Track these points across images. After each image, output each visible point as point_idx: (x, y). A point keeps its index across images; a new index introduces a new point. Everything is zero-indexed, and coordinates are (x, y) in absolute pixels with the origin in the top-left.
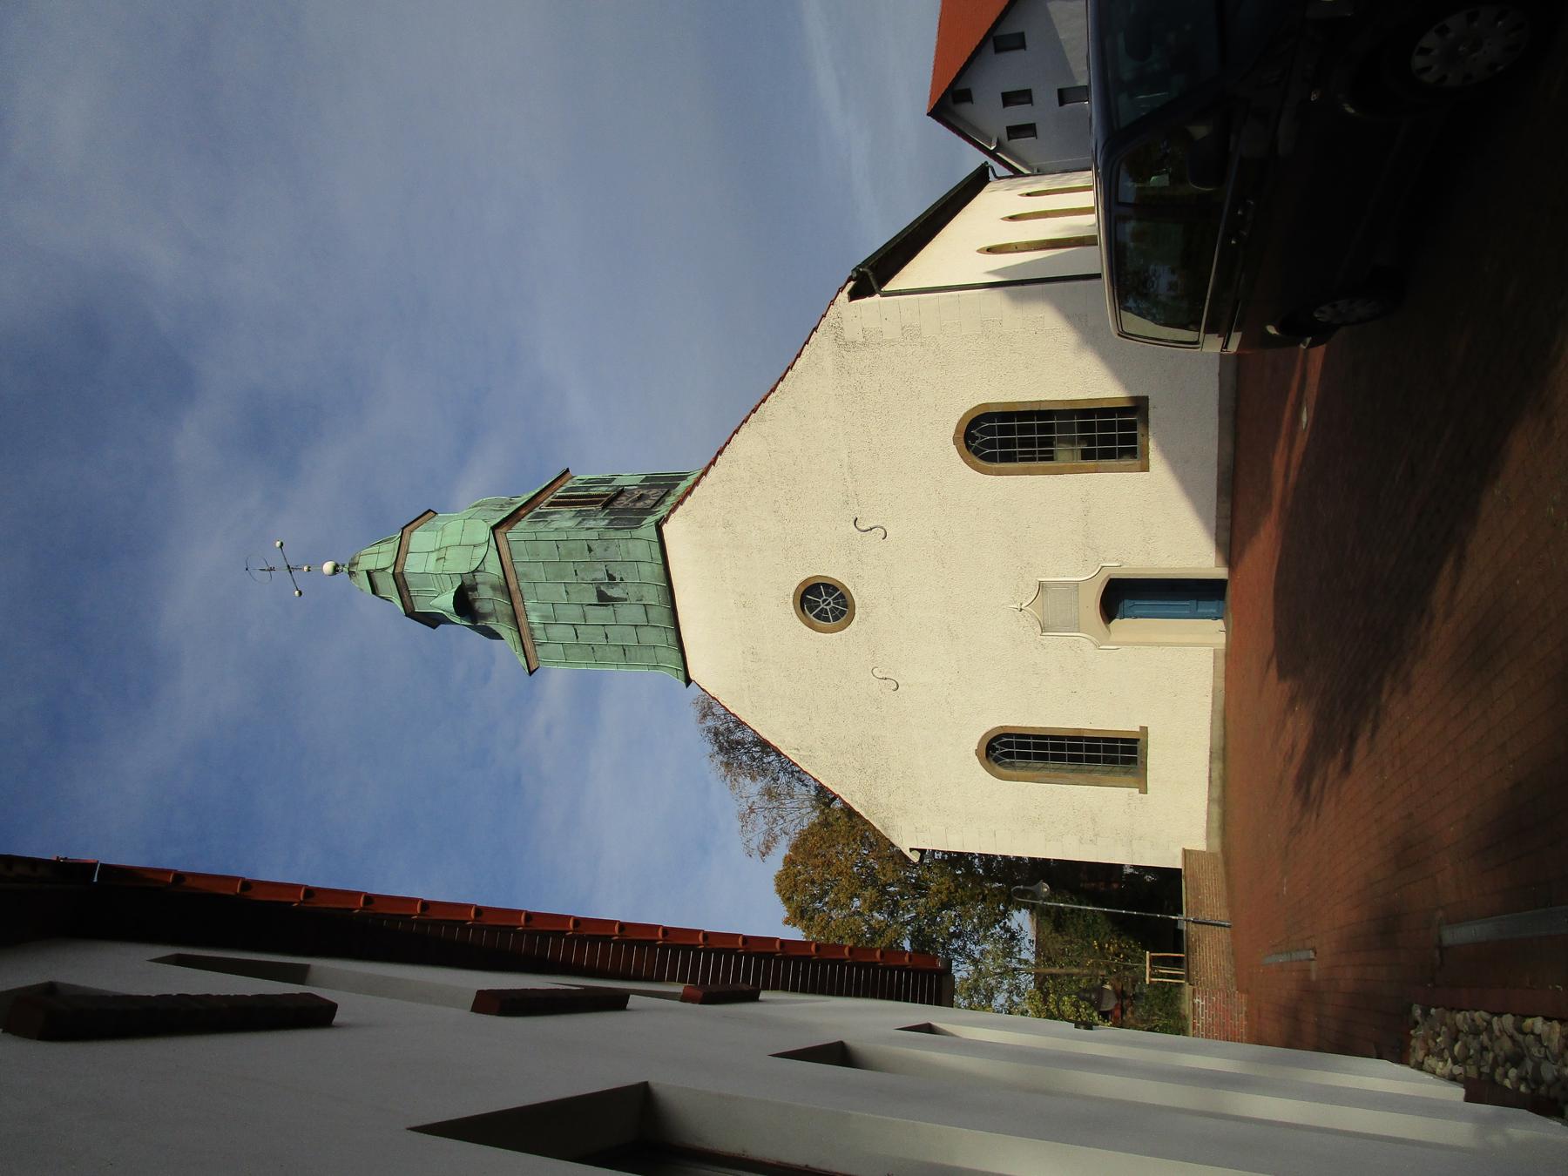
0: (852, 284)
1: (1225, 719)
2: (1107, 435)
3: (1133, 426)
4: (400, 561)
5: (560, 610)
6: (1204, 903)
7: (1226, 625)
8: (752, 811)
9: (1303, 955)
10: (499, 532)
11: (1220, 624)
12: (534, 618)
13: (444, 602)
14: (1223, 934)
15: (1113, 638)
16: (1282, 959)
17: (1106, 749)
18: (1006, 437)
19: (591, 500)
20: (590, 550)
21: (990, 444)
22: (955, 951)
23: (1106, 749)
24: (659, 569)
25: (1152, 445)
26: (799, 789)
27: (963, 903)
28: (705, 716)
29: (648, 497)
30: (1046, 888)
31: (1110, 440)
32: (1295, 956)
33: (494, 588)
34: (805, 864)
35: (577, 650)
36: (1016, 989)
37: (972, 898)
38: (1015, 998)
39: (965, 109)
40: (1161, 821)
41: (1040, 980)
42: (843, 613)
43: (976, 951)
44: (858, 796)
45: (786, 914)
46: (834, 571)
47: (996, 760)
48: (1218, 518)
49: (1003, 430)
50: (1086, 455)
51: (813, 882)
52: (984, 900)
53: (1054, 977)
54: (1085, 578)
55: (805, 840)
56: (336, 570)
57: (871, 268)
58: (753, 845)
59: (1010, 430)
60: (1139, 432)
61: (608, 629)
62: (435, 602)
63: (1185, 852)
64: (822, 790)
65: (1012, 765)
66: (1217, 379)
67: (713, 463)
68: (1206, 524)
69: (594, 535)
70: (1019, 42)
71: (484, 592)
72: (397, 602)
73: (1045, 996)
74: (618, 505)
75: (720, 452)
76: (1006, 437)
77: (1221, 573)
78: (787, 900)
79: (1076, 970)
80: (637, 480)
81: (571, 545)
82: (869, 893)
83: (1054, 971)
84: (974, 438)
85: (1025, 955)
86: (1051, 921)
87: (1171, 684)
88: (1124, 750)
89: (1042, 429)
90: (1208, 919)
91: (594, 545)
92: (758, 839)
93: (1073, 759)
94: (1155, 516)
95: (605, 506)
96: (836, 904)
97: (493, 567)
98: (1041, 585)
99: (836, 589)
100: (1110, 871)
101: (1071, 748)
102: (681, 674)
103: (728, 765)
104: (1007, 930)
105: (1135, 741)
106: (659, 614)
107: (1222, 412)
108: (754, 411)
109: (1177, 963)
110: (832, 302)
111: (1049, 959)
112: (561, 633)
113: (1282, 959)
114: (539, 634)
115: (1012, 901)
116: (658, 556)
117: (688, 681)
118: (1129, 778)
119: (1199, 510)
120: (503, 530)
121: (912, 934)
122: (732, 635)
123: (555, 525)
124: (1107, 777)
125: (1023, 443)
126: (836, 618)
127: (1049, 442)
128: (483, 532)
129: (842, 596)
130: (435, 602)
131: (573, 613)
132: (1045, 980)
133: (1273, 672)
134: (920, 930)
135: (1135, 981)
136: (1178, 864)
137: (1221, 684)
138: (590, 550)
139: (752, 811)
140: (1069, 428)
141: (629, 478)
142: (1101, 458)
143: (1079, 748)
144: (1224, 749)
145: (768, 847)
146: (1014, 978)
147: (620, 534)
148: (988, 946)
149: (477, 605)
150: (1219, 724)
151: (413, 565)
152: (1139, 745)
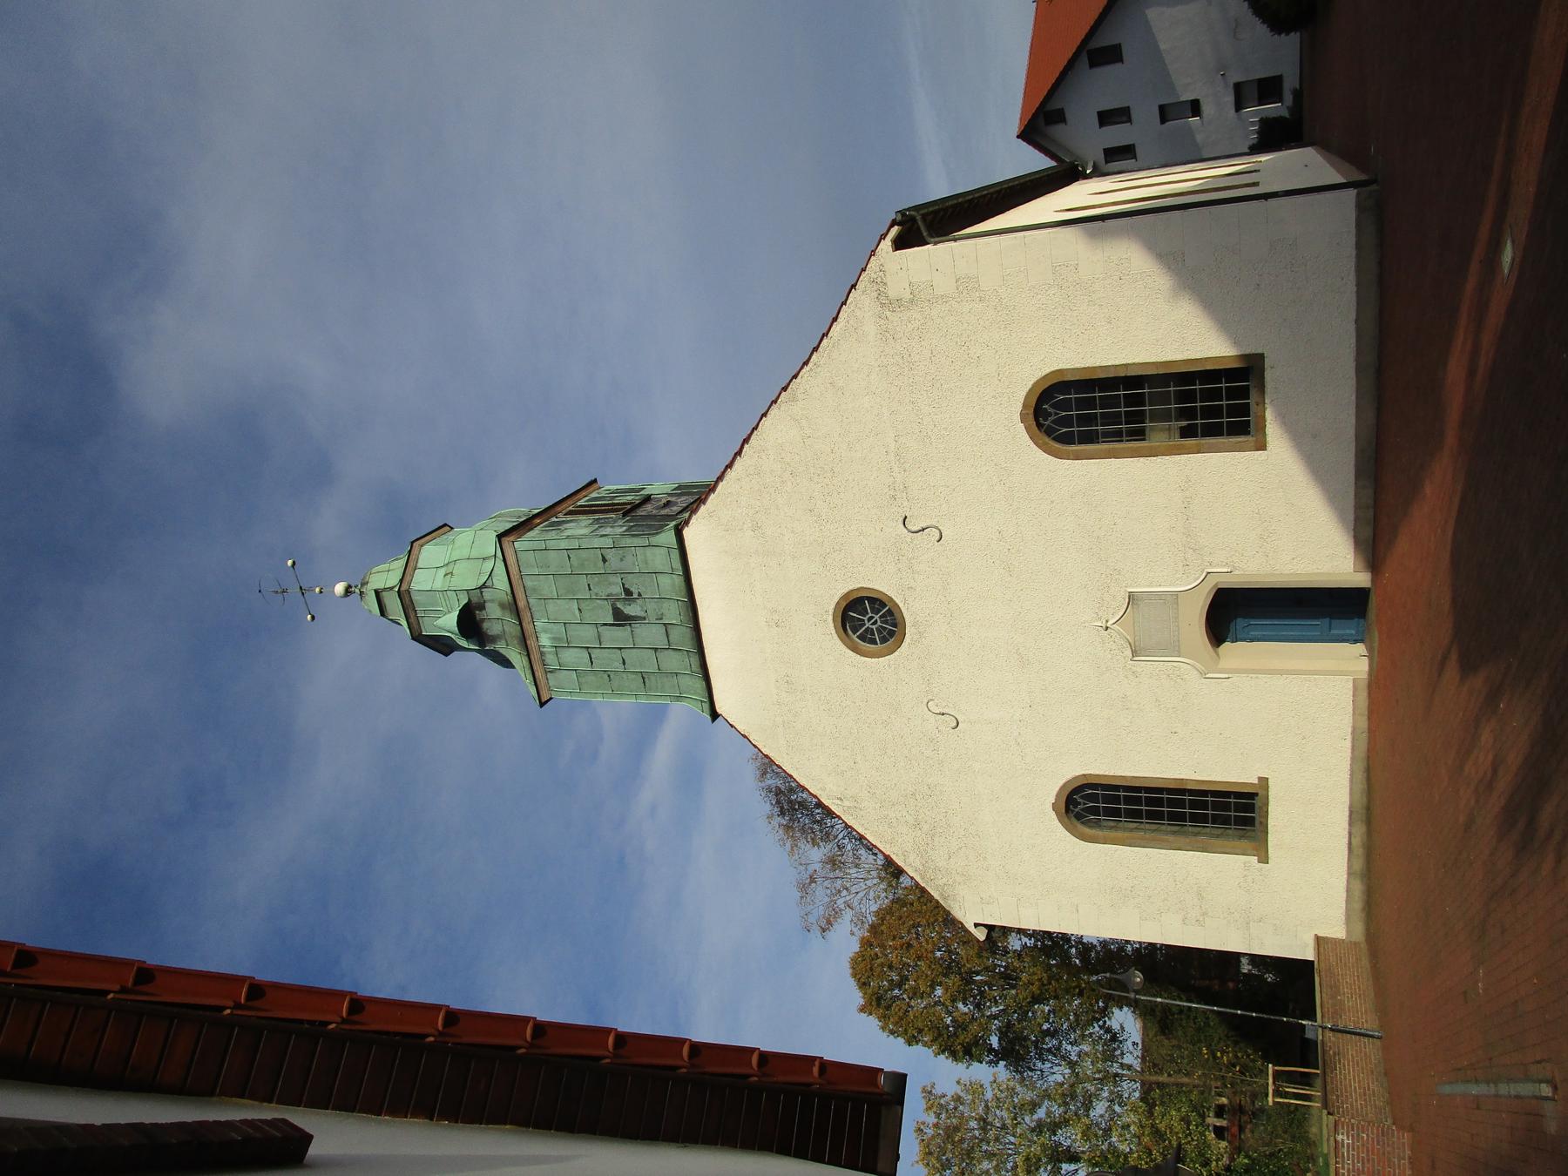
0: (895, 229)
1: (1368, 770)
2: (1209, 405)
3: (1244, 393)
4: (407, 578)
5: (575, 631)
6: (1345, 1004)
7: (1370, 649)
8: (813, 880)
9: (1525, 1089)
11: (1360, 648)
12: (545, 640)
13: (447, 623)
14: (1371, 1049)
15: (1223, 664)
16: (1475, 1090)
17: (1216, 806)
18: (1084, 412)
19: (612, 508)
20: (604, 560)
21: (1066, 421)
22: (1049, 1050)
23: (1216, 806)
24: (679, 581)
25: (1269, 415)
27: (1056, 997)
28: (764, 773)
29: (675, 504)
30: (1138, 978)
32: (1504, 1089)
33: (502, 606)
34: (883, 946)
35: (591, 678)
36: (1116, 1098)
37: (1067, 991)
38: (1117, 1108)
39: (1058, 131)
40: (1290, 898)
41: (1147, 1089)
42: (892, 634)
43: (1073, 1052)
46: (910, 611)
47: (1079, 817)
48: (1357, 507)
49: (1082, 404)
50: (1186, 433)
51: (890, 967)
52: (1081, 994)
53: (1161, 1085)
54: (1189, 583)
55: (883, 919)
56: (348, 591)
57: (924, 217)
58: (812, 919)
59: (1090, 403)
60: (1253, 400)
61: (625, 654)
62: (440, 622)
63: (1318, 939)
64: (889, 861)
65: (1097, 824)
66: (1352, 327)
67: (739, 453)
68: (1342, 518)
69: (608, 542)
70: (1112, 55)
72: (404, 623)
73: (1151, 1107)
74: (641, 512)
75: (746, 441)
76: (1084, 412)
77: (1362, 579)
78: (863, 985)
79: (1186, 1080)
80: (668, 488)
81: (583, 554)
82: (953, 981)
83: (1163, 1078)
84: (1047, 415)
85: (1128, 1059)
86: (1159, 1022)
87: (1298, 722)
88: (1239, 807)
89: (1130, 400)
90: (1351, 1026)
91: (610, 555)
92: (819, 911)
93: (1174, 817)
94: (1275, 508)
95: (624, 515)
96: (915, 993)
97: (501, 582)
100: (1229, 960)
101: (1171, 803)
102: (706, 706)
103: (788, 828)
104: (1108, 1030)
105: (1252, 796)
106: (681, 635)
107: (1359, 369)
108: (785, 389)
109: (1305, 1080)
110: (873, 253)
111: (1155, 1065)
113: (1475, 1090)
114: (551, 659)
115: (1118, 996)
116: (677, 565)
117: (715, 715)
118: (1244, 843)
119: (1332, 498)
120: (512, 538)
121: (999, 1029)
122: (765, 663)
123: (568, 533)
124: (1219, 842)
126: (884, 640)
128: (490, 546)
129: (890, 612)
130: (440, 622)
131: (587, 634)
132: (1150, 1089)
133: (1452, 671)
134: (1009, 1025)
135: (1254, 1096)
137: (1363, 723)
138: (604, 560)
139: (813, 880)
140: (1165, 398)
141: (659, 488)
142: (1204, 435)
143: (1181, 804)
144: (1368, 808)
145: (829, 923)
146: (1115, 1084)
148: (1086, 1048)
149: (485, 625)
150: (1360, 776)
151: (421, 581)
152: (1258, 802)
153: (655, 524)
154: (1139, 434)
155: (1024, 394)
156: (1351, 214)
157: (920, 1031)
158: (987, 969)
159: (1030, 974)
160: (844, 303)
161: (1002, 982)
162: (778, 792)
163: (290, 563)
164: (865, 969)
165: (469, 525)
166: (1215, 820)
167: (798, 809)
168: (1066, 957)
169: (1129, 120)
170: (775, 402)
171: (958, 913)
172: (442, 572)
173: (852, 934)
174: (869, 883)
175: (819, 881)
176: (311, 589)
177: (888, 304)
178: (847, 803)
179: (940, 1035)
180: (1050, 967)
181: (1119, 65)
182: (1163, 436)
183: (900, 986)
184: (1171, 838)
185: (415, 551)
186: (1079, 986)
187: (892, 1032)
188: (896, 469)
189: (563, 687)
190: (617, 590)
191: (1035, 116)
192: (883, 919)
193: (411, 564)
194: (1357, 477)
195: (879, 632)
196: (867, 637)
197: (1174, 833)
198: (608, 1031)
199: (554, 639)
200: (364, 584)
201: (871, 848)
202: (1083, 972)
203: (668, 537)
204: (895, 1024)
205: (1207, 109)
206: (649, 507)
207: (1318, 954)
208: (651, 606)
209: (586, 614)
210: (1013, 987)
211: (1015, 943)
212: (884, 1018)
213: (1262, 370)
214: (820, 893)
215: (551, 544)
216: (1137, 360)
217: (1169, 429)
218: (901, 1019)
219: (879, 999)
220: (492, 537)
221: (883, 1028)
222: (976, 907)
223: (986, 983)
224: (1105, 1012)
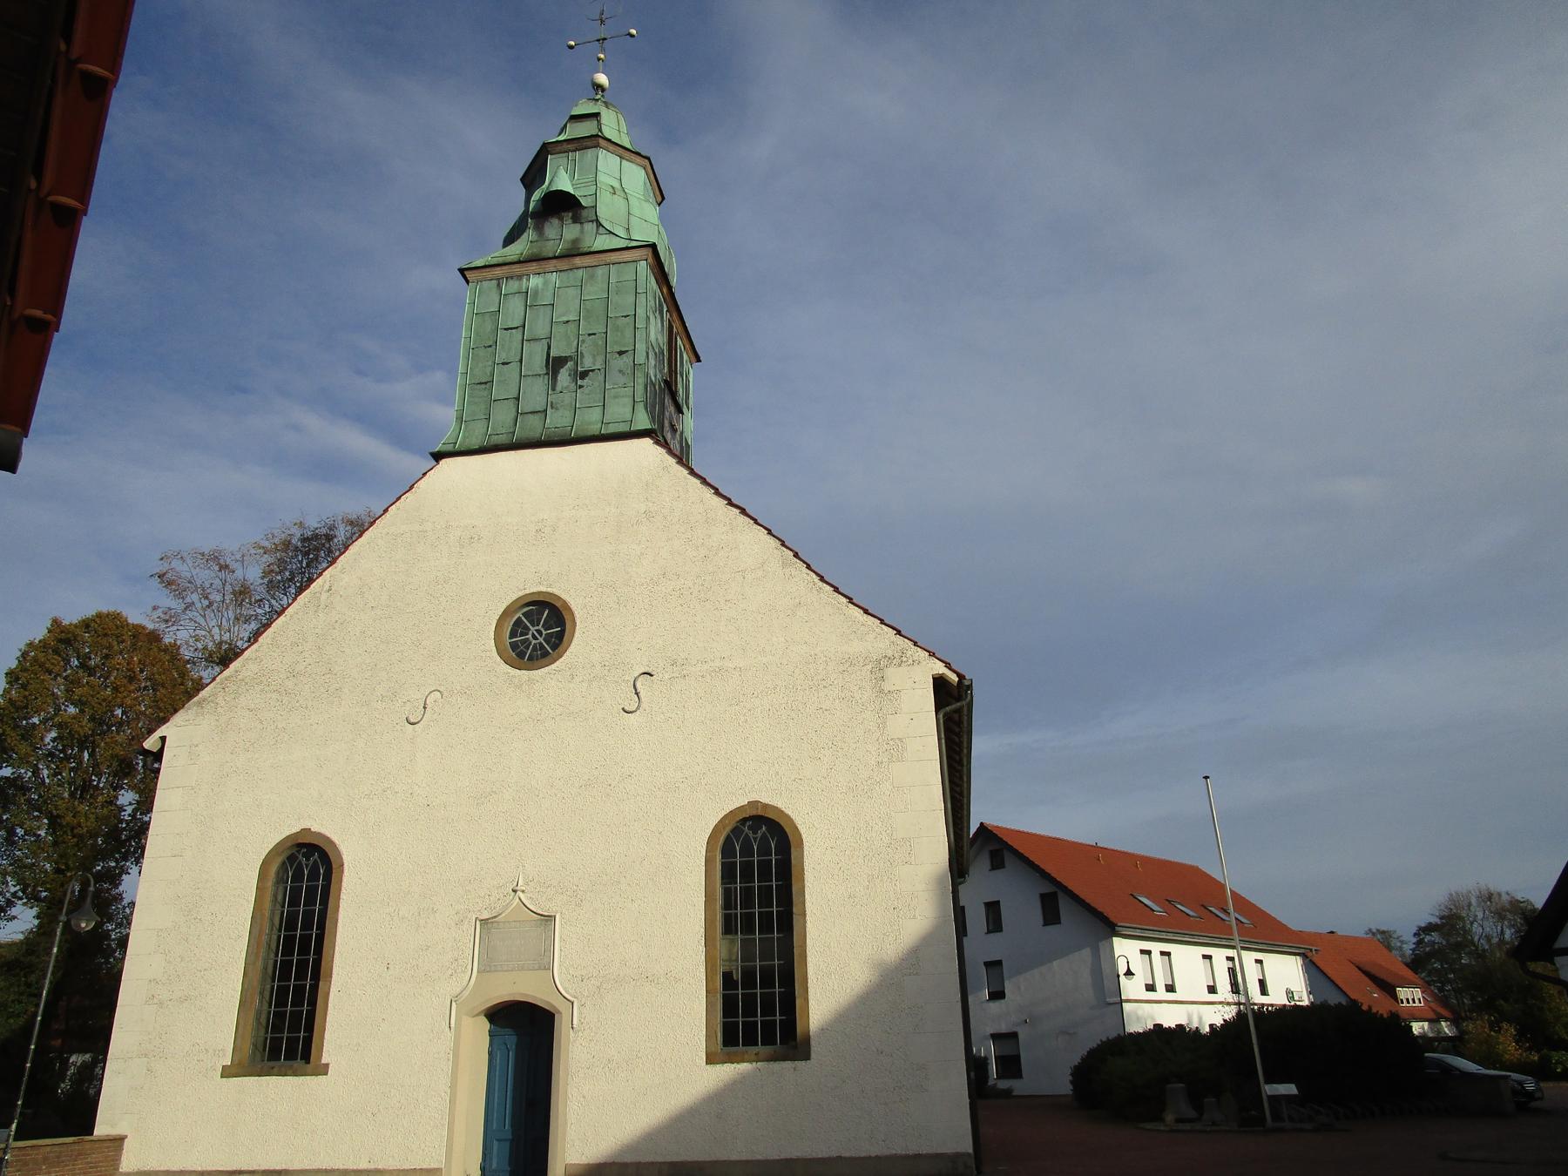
2: (757, 1002)
3: (768, 1040)
4: (611, 147)
10: (648, 252)
12: (535, 281)
13: (561, 179)
15: (468, 1022)
17: (296, 1016)
18: (757, 869)
19: (673, 371)
20: (621, 353)
23: (296, 1016)
24: (594, 429)
25: (744, 1067)
26: (247, 630)
27: (55, 843)
31: (750, 1010)
33: (576, 241)
35: (489, 326)
42: (521, 655)
44: (253, 667)
45: (66, 622)
46: (579, 648)
47: (291, 859)
50: (727, 977)
52: (58, 871)
54: (563, 981)
56: (598, 87)
58: (176, 564)
60: (760, 1049)
61: (514, 366)
63: (120, 1140)
65: (280, 880)
67: (731, 503)
69: (640, 359)
70: (1051, 915)
71: (571, 231)
72: (561, 138)
74: (668, 401)
75: (743, 511)
76: (757, 869)
78: (86, 624)
80: (688, 435)
81: (629, 332)
82: (86, 726)
88: (292, 1043)
91: (627, 359)
92: (183, 569)
95: (666, 381)
96: (72, 683)
97: (602, 242)
98: (549, 919)
99: (555, 647)
101: (302, 965)
102: (450, 448)
103: (287, 544)
105: (306, 1057)
106: (533, 427)
108: (796, 555)
110: (932, 654)
112: (514, 311)
114: (513, 286)
116: (612, 429)
117: (438, 457)
118: (247, 1048)
119: (652, 1137)
120: (650, 260)
121: (20, 777)
125: (747, 894)
126: (514, 646)
127: (748, 928)
128: (643, 234)
129: (545, 654)
130: (562, 171)
131: (540, 327)
136: (101, 1130)
138: (621, 353)
141: (688, 423)
143: (301, 975)
147: (640, 389)
149: (555, 221)
152: (298, 1063)
153: (657, 415)
154: (728, 928)
155: (780, 806)
156: (949, 1148)
157: (24, 687)
158: (96, 765)
159: (86, 815)
160: (882, 622)
161: (79, 782)
162: (329, 538)
163: (634, 32)
164: (107, 628)
165: (661, 217)
166: (279, 1016)
167: (307, 556)
168: (104, 855)
169: (1046, 923)
170: (783, 544)
171: (178, 718)
172: (616, 184)
173: (155, 608)
174: (216, 630)
175: (222, 574)
176: (603, 51)
177: (880, 667)
178: (324, 596)
179: (18, 709)
180: (94, 836)
181: (1040, 920)
182: (724, 955)
183: (83, 666)
184: (260, 964)
185: (639, 160)
186: (68, 869)
187: (24, 655)
188: (706, 667)
189: (483, 295)
190: (587, 363)
191: (1000, 840)
192: (166, 650)
193: (627, 154)
194: (672, 1164)
195: (523, 642)
196: (518, 629)
197: (265, 968)
198: (115, 68)
199: (536, 293)
200: (606, 104)
201: (255, 637)
202: (95, 854)
203: (643, 422)
204: (35, 659)
205: (995, 1006)
206: (672, 409)
207: (101, 1140)
208: (567, 398)
209: (562, 328)
210: (72, 795)
211: (127, 798)
212: (44, 644)
213: (793, 1059)
214: (206, 575)
215: (642, 299)
216: (809, 925)
217: (730, 960)
218: (42, 665)
219: (67, 642)
220: (653, 239)
221: (31, 645)
222: (184, 740)
223: (81, 762)
224: (33, 898)
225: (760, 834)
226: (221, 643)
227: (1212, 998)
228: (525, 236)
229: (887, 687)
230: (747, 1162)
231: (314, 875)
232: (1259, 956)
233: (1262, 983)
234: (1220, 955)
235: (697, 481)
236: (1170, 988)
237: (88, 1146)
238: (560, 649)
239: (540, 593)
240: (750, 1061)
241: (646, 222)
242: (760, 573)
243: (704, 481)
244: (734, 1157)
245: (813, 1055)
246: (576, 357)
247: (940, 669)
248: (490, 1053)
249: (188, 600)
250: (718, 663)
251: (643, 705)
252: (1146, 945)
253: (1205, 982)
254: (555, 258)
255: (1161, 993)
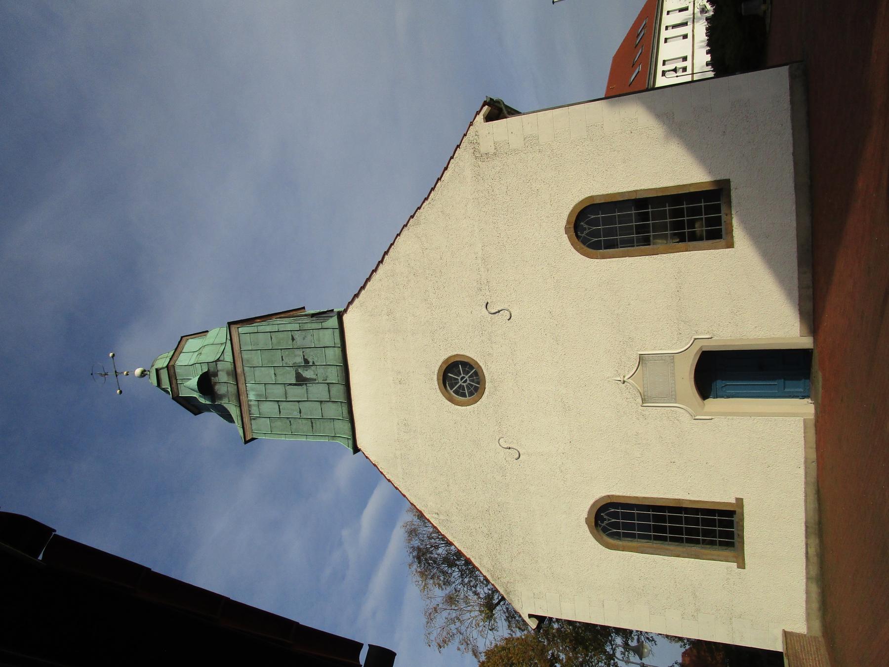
10: (233, 328)
12: (252, 396)
13: (190, 386)
18: (609, 225)
20: (293, 339)
24: (338, 351)
25: (735, 222)
33: (228, 374)
35: (278, 423)
46: (471, 352)
47: (605, 530)
54: (680, 346)
61: (302, 405)
63: (786, 634)
67: (381, 262)
71: (223, 377)
75: (386, 253)
76: (609, 225)
81: (280, 335)
88: (722, 524)
91: (297, 335)
97: (228, 357)
98: (641, 358)
99: (471, 367)
102: (351, 442)
103: (422, 574)
105: (731, 513)
106: (338, 392)
108: (412, 217)
110: (471, 124)
112: (269, 408)
114: (254, 410)
116: (338, 341)
117: (356, 450)
126: (471, 394)
129: (476, 374)
136: (779, 647)
138: (293, 339)
149: (217, 387)
152: (735, 519)
160: (452, 158)
162: (419, 549)
163: (111, 354)
170: (406, 226)
174: (473, 614)
177: (480, 156)
178: (442, 517)
185: (183, 342)
188: (482, 269)
190: (299, 360)
193: (179, 349)
196: (460, 392)
199: (258, 395)
200: (153, 366)
213: (729, 191)
214: (440, 620)
216: (643, 188)
225: (586, 226)
226: (481, 611)
227: (690, 36)
228: (225, 405)
229: (492, 151)
230: (797, 216)
231: (615, 515)
232: (665, 13)
233: (681, 10)
234: (664, 34)
235: (369, 283)
236: (685, 59)
237: (790, 652)
238: (472, 363)
239: (438, 379)
240: (732, 218)
241: (218, 334)
242: (423, 239)
243: (368, 280)
244: (794, 224)
245: (727, 178)
246: (296, 366)
247: (480, 118)
248: (728, 397)
249: (455, 631)
250: (479, 261)
251: (506, 306)
252: (659, 73)
253: (681, 41)
254: (237, 384)
255: (688, 64)
